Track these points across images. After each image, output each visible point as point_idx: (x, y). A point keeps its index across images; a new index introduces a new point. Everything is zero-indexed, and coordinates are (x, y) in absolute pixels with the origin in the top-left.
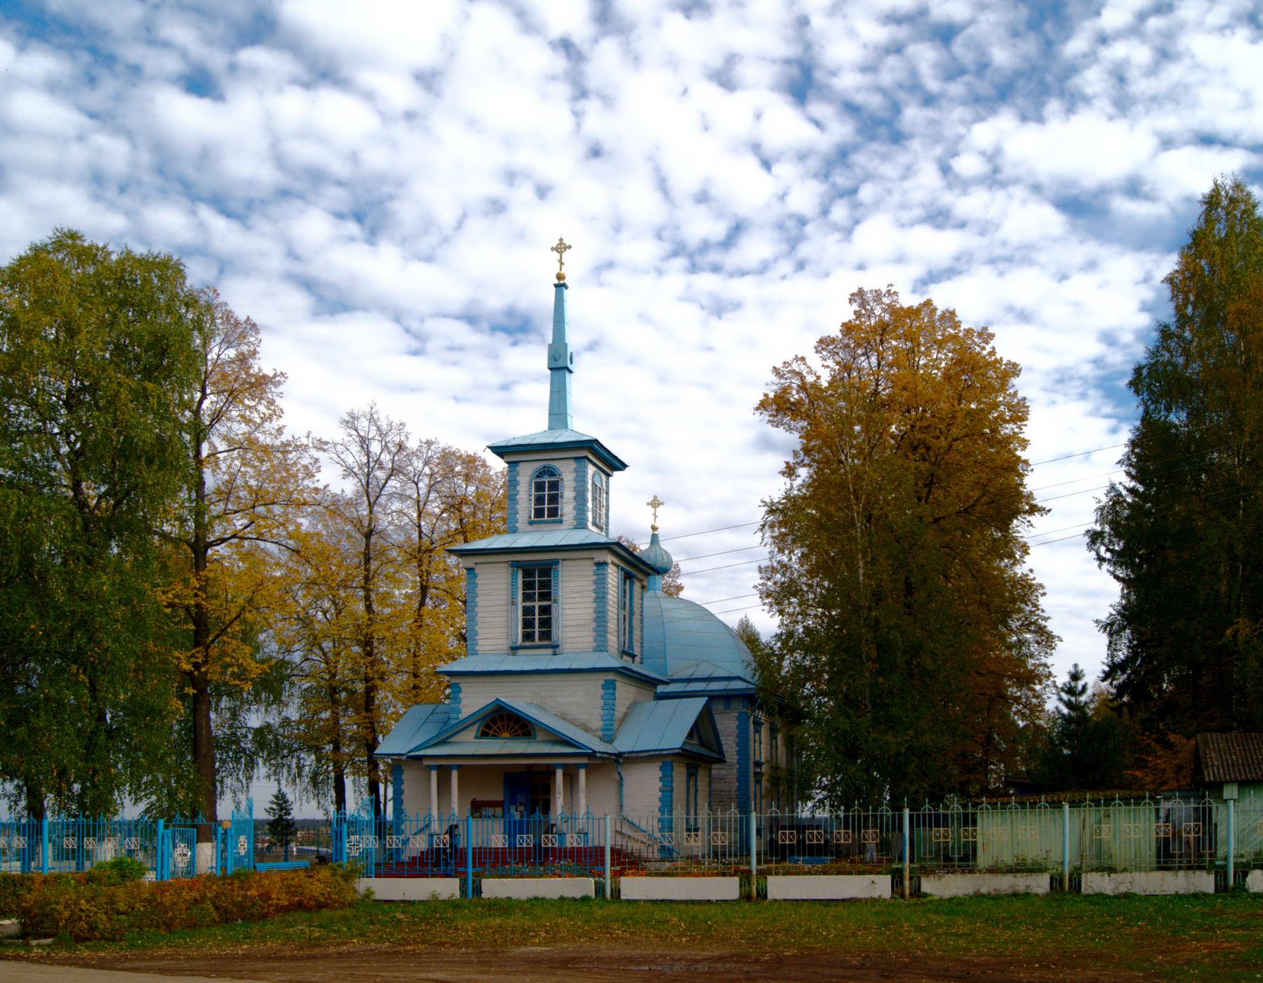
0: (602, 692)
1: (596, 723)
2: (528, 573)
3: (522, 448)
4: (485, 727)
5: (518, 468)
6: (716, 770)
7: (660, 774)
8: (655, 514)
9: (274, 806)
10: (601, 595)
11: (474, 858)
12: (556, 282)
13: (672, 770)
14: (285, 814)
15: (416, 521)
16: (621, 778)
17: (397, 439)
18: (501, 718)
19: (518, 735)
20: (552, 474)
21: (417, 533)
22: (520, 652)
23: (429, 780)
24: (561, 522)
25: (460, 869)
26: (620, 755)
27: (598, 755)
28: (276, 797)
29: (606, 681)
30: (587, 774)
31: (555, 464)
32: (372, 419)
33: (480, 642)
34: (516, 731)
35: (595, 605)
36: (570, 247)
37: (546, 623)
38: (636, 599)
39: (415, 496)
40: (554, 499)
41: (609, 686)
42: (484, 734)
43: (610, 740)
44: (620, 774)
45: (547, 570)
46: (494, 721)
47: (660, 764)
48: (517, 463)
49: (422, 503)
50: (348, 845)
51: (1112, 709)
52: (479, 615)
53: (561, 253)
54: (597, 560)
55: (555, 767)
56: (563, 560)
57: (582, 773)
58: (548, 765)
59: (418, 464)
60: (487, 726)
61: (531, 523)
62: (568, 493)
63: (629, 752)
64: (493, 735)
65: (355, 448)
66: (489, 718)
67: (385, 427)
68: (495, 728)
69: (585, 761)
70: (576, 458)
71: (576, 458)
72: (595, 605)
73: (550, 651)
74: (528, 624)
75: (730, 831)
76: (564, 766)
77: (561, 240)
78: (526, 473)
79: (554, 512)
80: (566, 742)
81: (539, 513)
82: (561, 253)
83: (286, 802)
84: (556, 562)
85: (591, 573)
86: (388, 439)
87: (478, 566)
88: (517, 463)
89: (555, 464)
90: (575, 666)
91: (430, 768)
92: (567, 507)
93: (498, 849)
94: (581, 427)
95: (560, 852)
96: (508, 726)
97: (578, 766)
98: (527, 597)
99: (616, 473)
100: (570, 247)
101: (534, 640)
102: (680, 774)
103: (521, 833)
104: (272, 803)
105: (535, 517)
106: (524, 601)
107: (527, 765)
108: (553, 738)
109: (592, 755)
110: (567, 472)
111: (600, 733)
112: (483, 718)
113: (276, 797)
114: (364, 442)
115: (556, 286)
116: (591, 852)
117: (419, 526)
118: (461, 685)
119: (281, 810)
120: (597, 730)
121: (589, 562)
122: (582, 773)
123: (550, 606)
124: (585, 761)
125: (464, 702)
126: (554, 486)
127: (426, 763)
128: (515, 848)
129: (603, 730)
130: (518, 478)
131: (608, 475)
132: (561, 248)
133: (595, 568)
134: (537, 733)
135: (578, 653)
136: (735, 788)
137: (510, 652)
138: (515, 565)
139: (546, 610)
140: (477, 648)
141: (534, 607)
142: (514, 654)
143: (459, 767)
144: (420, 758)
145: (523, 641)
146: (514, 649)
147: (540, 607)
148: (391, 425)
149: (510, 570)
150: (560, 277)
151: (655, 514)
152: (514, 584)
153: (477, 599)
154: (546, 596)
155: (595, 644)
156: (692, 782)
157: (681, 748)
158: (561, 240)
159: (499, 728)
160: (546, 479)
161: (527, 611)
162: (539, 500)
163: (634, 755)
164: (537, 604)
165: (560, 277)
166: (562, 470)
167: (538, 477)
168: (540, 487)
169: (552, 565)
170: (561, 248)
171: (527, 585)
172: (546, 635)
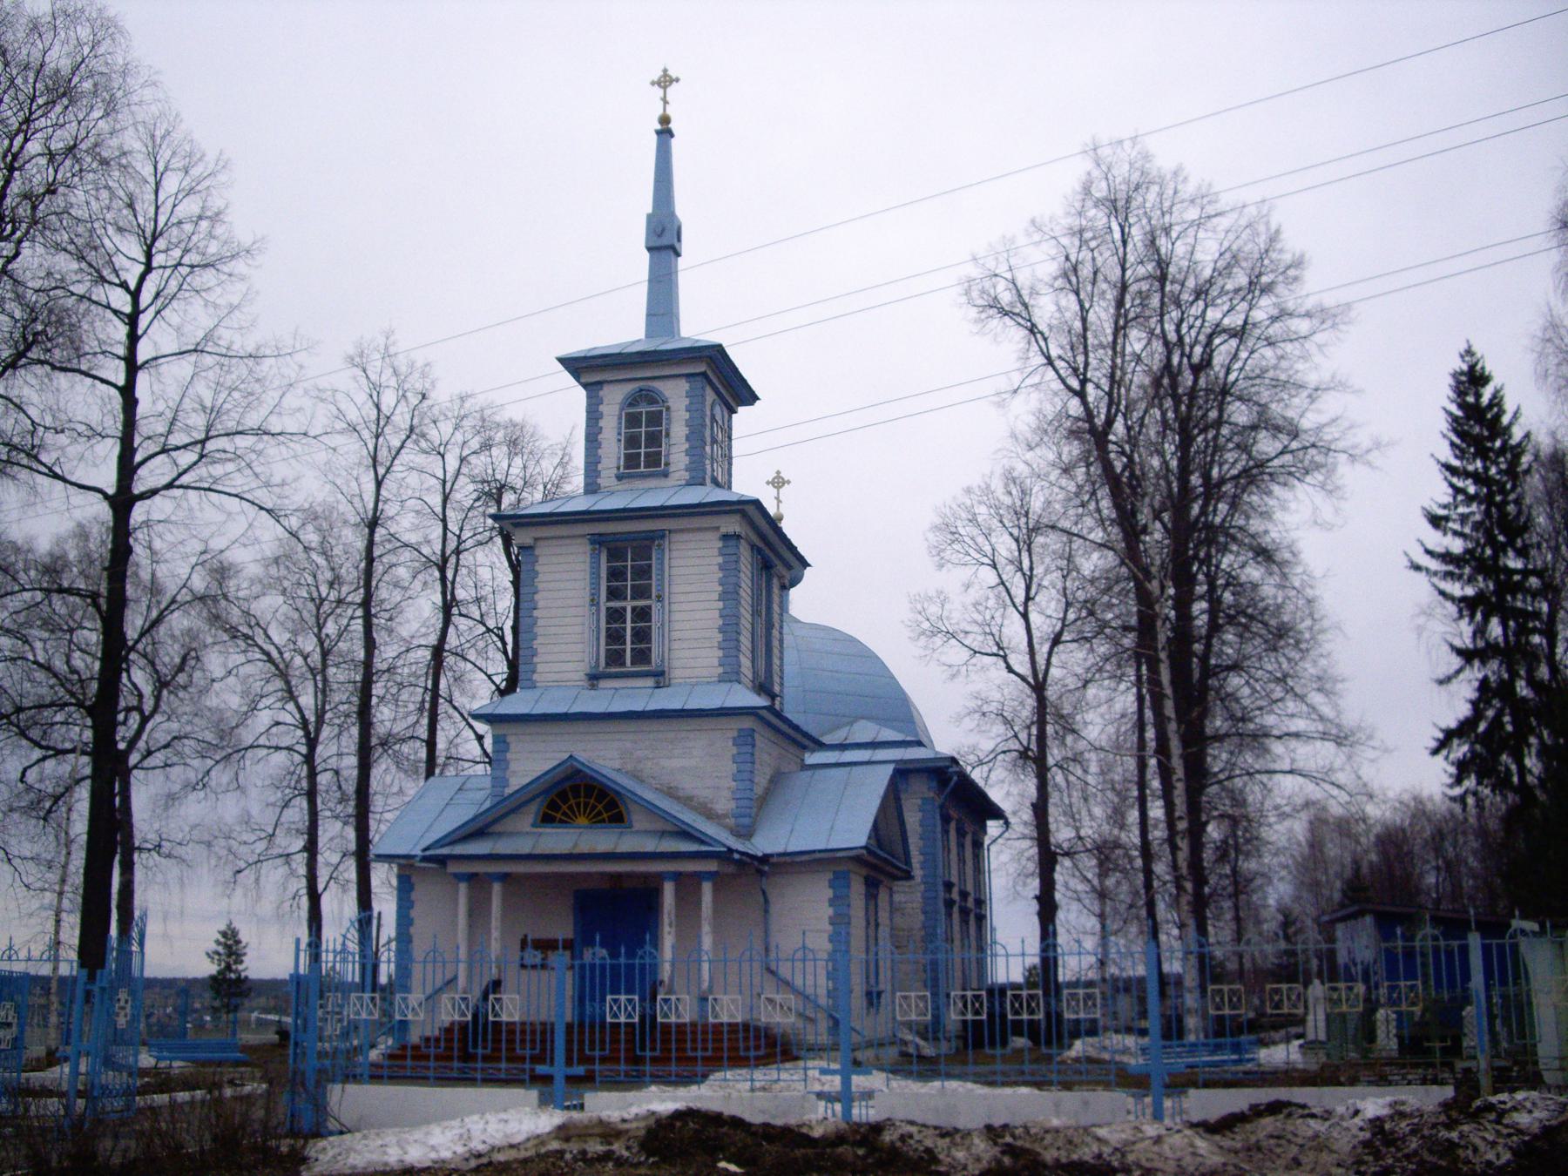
0: (735, 750)
1: (724, 804)
2: (615, 554)
3: (608, 361)
4: (549, 807)
5: (601, 393)
6: (900, 886)
7: (830, 893)
8: (777, 498)
9: (221, 949)
10: (731, 589)
11: (569, 1042)
12: (659, 127)
13: (849, 887)
14: (236, 962)
15: (438, 510)
16: (766, 901)
17: (419, 386)
18: (575, 790)
19: (603, 821)
20: (653, 401)
21: (440, 530)
22: (603, 684)
23: (455, 901)
24: (666, 475)
25: (541, 1069)
26: (765, 859)
27: (736, 856)
28: (224, 934)
29: (740, 730)
30: (716, 890)
31: (658, 385)
32: (387, 355)
33: (540, 668)
34: (599, 813)
35: (721, 604)
36: (677, 80)
37: (642, 636)
38: (776, 598)
39: (440, 474)
40: (654, 439)
41: (745, 740)
42: (546, 819)
43: (746, 833)
44: (764, 893)
45: (646, 545)
46: (563, 796)
47: (830, 876)
48: (600, 383)
49: (448, 486)
50: (320, 1013)
51: (1453, 799)
52: (540, 622)
53: (665, 88)
54: (723, 530)
55: (661, 877)
56: (676, 531)
57: (707, 888)
58: (647, 876)
59: (446, 428)
60: (553, 805)
61: (619, 478)
62: (678, 430)
63: (780, 855)
64: (562, 821)
65: (361, 397)
66: (555, 791)
67: (403, 369)
68: (565, 807)
69: (712, 866)
70: (688, 376)
71: (688, 376)
72: (721, 604)
73: (650, 682)
74: (615, 637)
75: (1425, 976)
76: (677, 877)
77: (665, 71)
78: (614, 398)
79: (654, 460)
80: (686, 834)
81: (631, 461)
82: (665, 88)
83: (238, 942)
84: (661, 535)
85: (716, 552)
86: (406, 386)
87: (540, 543)
88: (600, 383)
89: (657, 385)
90: (693, 704)
91: (460, 877)
92: (677, 453)
93: (514, 1023)
94: (695, 327)
95: (694, 1032)
96: (586, 805)
97: (698, 877)
98: (614, 594)
99: (741, 409)
100: (677, 80)
101: (623, 664)
102: (857, 889)
103: (616, 991)
104: (218, 943)
105: (626, 467)
106: (608, 599)
107: (602, 874)
108: (660, 826)
109: (727, 855)
110: (676, 395)
111: (731, 821)
112: (546, 792)
113: (224, 934)
114: (376, 389)
115: (658, 133)
116: (533, 1032)
117: (444, 521)
118: (509, 739)
119: (229, 955)
120: (725, 816)
121: (709, 535)
122: (707, 888)
123: (650, 607)
124: (712, 866)
125: (513, 766)
126: (655, 419)
127: (453, 868)
128: (603, 1022)
129: (736, 817)
130: (601, 408)
131: (732, 411)
132: (665, 81)
133: (720, 544)
134: (635, 817)
135: (693, 685)
136: (919, 925)
137: (586, 684)
138: (598, 541)
139: (643, 614)
140: (535, 677)
141: (624, 609)
142: (593, 687)
143: (504, 877)
144: (442, 861)
145: (608, 664)
146: (594, 678)
147: (634, 609)
148: (412, 365)
149: (588, 548)
150: (665, 120)
151: (777, 498)
152: (595, 575)
153: (537, 597)
154: (642, 592)
155: (721, 670)
156: (872, 907)
157: (865, 848)
158: (665, 71)
159: (570, 808)
160: (644, 409)
161: (615, 616)
162: (632, 441)
163: (788, 859)
164: (629, 605)
165: (665, 120)
166: (667, 394)
167: (630, 405)
168: (633, 420)
169: (653, 539)
170: (665, 81)
171: (615, 574)
172: (642, 656)
